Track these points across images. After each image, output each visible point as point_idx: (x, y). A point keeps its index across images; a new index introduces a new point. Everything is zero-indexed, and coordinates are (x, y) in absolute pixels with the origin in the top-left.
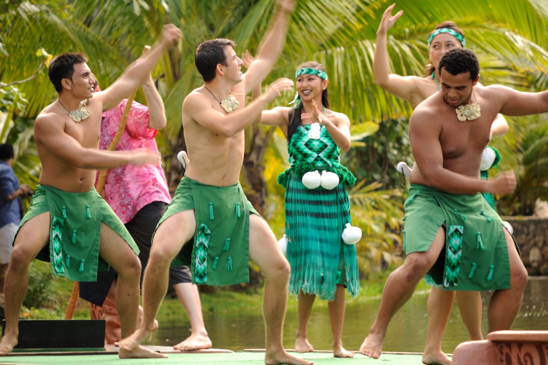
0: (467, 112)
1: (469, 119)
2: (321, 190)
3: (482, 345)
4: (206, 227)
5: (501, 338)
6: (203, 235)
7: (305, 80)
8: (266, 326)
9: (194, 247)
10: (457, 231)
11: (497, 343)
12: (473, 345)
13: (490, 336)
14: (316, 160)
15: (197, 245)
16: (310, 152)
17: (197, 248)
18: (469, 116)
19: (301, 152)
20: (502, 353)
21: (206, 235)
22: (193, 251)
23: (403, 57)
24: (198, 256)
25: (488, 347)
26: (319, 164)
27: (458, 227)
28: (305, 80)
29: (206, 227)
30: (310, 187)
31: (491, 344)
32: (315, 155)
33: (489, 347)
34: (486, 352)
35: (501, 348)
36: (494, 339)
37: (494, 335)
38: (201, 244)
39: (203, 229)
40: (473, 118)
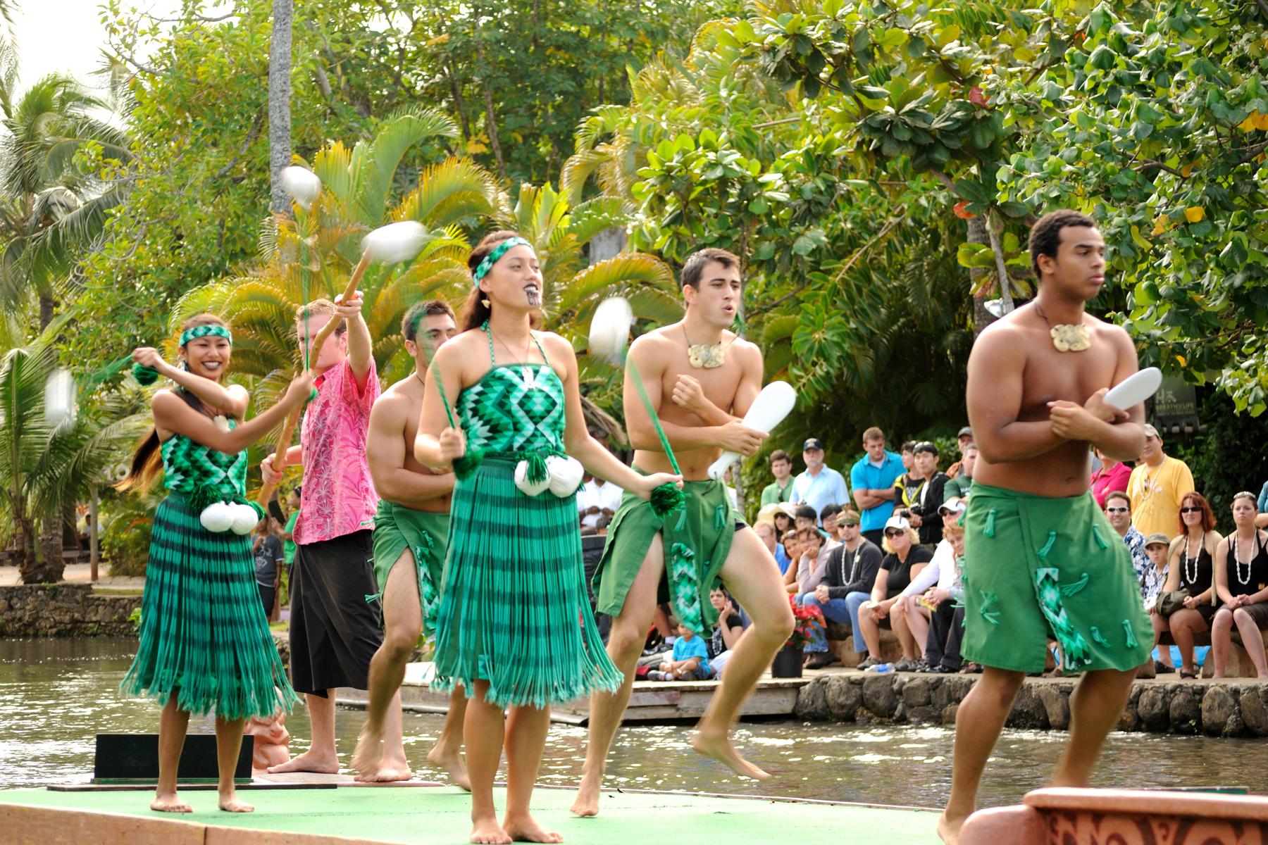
0: (1069, 335)
1: (1074, 348)
2: (229, 536)
3: (1016, 816)
4: (683, 546)
5: (1056, 804)
6: (682, 561)
7: (213, 346)
8: (834, 738)
9: (670, 582)
10: (1048, 577)
11: (1047, 814)
12: (1001, 815)
13: (1031, 798)
14: (222, 482)
15: (675, 578)
16: (214, 468)
17: (677, 584)
18: (29, 461)
19: (199, 468)
20: (1055, 832)
21: (689, 559)
22: (671, 589)
23: (420, 298)
24: (680, 595)
25: (1028, 819)
26: (226, 489)
27: (1050, 570)
28: (213, 346)
29: (683, 546)
30: (212, 528)
31: (1034, 813)
32: (222, 474)
33: (1030, 820)
34: (1024, 828)
35: (1054, 822)
36: (1041, 804)
37: (1039, 797)
38: (682, 576)
39: (679, 551)
40: (1079, 347)
